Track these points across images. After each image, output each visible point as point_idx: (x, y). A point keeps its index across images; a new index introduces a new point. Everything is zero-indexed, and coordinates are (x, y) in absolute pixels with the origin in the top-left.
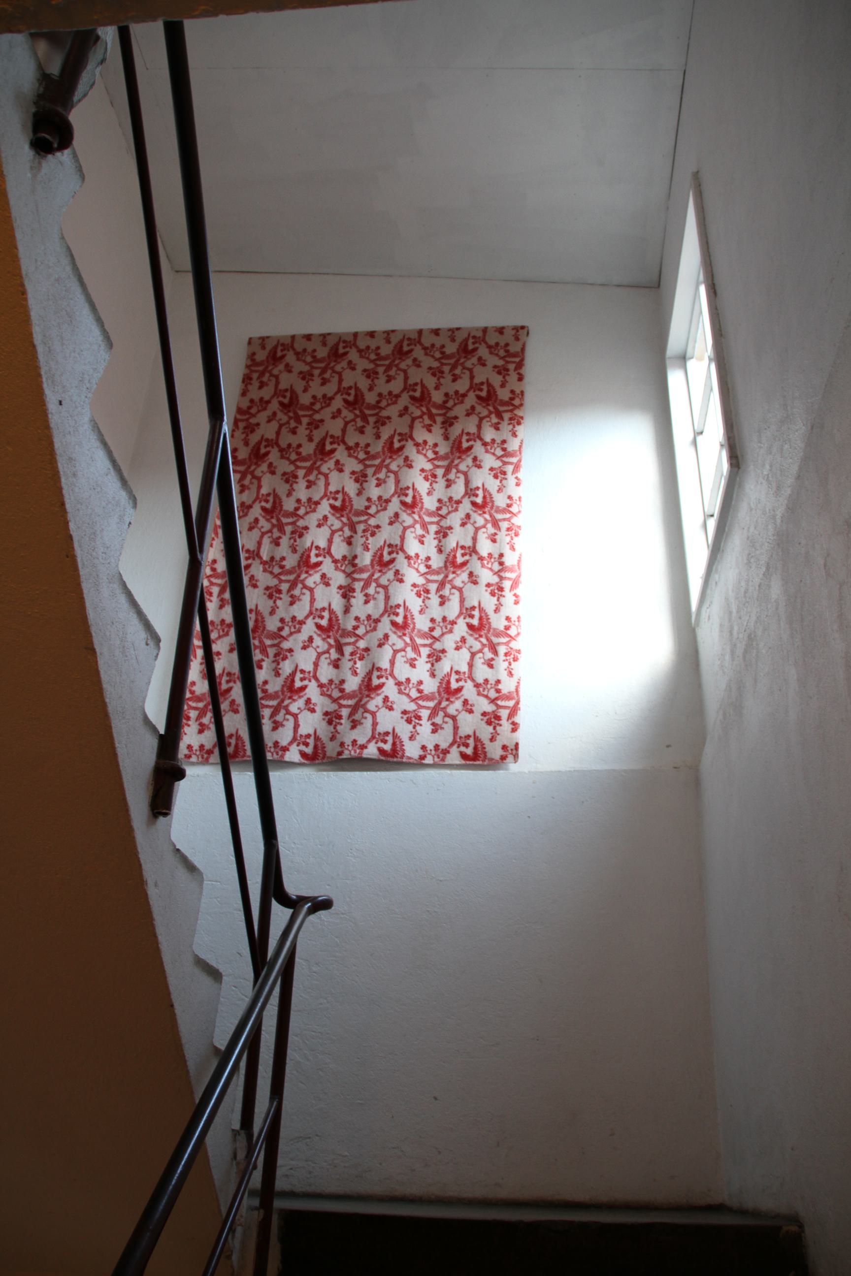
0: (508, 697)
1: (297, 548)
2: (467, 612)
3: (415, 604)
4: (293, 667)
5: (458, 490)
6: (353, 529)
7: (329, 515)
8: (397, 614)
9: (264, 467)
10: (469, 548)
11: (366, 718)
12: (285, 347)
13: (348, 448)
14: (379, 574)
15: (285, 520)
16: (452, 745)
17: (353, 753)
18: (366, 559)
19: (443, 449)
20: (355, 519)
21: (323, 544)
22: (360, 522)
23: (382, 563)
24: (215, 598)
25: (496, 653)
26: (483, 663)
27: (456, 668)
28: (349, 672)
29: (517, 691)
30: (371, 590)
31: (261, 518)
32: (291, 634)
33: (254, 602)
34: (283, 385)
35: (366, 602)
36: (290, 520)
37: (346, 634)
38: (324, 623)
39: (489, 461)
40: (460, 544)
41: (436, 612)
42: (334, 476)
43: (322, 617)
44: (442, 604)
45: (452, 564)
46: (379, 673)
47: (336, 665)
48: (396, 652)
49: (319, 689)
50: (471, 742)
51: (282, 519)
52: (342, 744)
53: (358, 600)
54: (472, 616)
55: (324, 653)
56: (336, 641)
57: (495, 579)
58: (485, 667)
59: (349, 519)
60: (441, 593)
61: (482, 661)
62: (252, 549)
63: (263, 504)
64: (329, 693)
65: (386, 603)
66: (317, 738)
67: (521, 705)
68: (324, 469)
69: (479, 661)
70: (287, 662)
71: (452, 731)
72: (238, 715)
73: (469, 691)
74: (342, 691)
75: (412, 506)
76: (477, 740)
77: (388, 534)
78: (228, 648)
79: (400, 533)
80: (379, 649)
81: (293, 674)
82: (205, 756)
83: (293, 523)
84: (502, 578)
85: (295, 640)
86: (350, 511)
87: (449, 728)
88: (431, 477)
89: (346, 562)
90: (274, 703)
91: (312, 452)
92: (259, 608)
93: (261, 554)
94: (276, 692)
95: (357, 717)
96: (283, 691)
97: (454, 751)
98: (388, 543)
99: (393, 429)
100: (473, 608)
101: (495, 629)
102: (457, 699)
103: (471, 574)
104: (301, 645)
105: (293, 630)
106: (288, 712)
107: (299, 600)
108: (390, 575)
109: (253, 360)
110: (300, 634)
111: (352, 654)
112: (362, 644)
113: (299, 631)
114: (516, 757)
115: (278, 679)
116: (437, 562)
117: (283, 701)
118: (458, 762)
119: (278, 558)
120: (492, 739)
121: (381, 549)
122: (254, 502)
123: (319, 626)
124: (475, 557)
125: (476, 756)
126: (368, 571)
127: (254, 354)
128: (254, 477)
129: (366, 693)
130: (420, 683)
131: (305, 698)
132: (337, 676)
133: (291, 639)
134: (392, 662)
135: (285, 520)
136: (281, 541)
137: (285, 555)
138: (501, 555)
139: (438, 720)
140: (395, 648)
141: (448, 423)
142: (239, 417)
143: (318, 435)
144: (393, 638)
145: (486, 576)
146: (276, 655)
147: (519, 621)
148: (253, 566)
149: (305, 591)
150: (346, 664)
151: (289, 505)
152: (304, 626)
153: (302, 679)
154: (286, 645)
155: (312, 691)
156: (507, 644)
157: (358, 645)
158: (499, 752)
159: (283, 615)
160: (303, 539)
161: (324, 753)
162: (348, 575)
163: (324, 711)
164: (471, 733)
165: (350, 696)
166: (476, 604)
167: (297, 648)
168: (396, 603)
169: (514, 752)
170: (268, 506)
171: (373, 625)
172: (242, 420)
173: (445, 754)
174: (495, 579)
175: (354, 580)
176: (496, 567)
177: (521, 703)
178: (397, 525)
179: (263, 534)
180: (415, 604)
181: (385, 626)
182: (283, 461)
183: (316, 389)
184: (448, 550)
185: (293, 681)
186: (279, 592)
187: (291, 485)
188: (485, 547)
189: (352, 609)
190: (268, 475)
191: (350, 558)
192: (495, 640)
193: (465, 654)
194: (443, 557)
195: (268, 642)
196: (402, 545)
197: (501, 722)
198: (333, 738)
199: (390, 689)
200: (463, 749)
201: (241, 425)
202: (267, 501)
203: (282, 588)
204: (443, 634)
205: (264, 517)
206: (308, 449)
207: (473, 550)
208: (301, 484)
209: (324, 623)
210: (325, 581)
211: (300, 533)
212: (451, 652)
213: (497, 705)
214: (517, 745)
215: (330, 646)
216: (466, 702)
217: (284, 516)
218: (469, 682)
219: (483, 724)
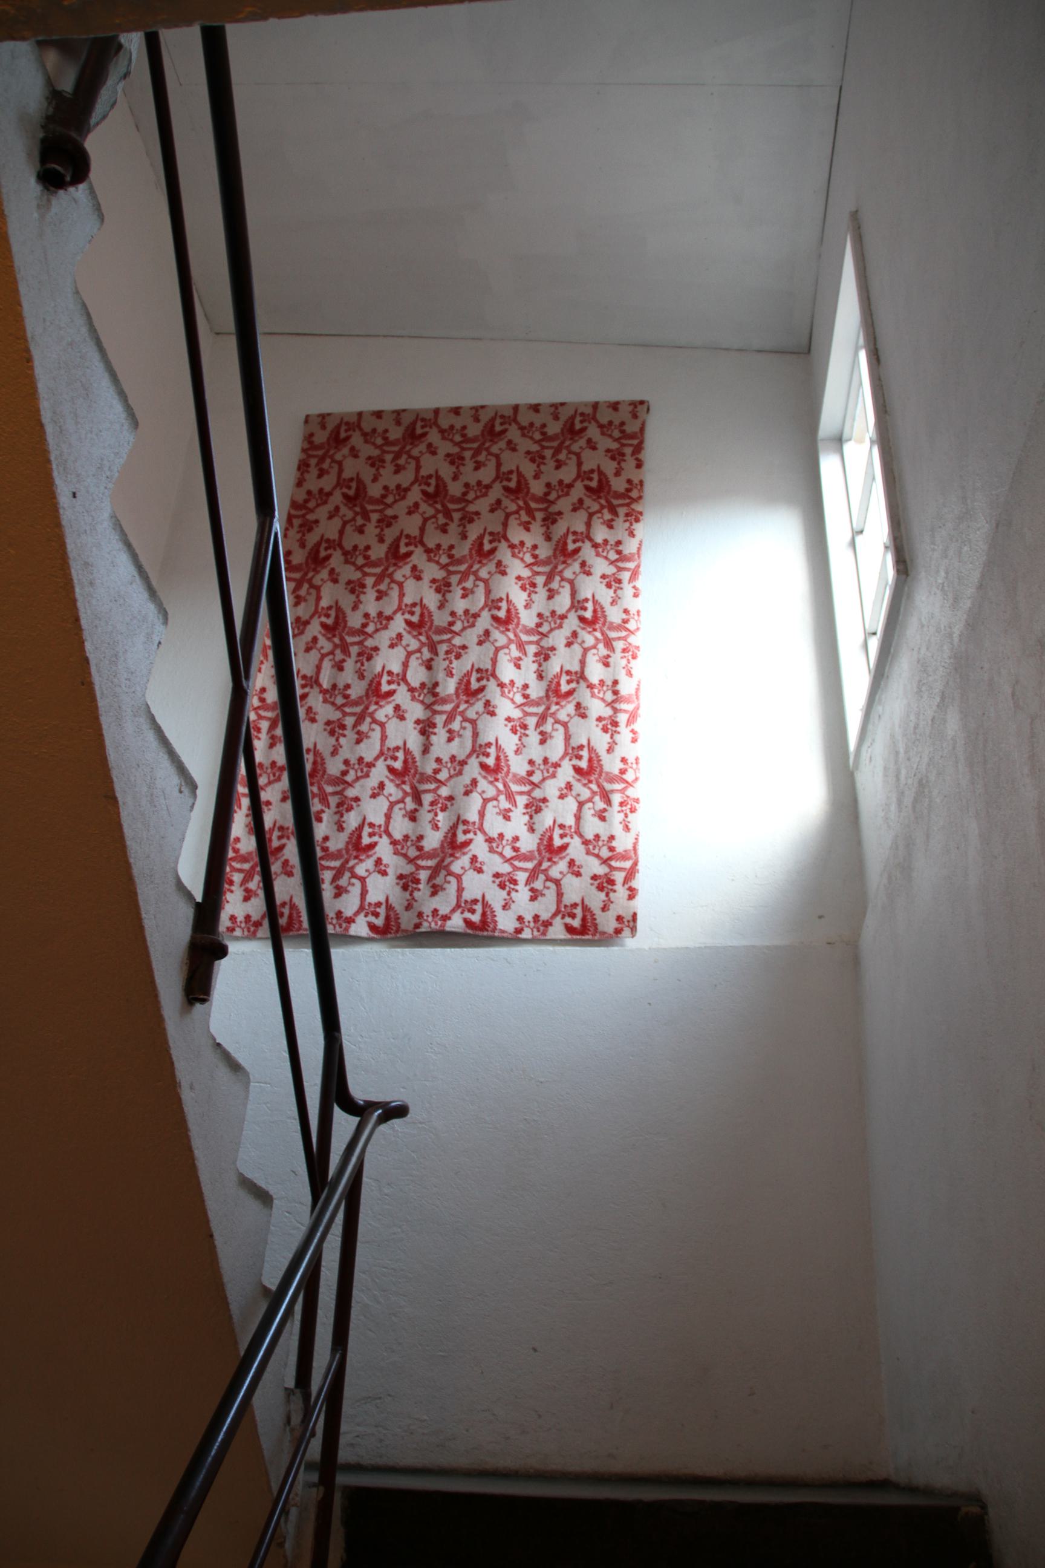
0: (624, 857)
1: (365, 674)
2: (573, 752)
3: (509, 742)
4: (360, 820)
5: (563, 602)
6: (433, 650)
7: (404, 633)
8: (488, 755)
9: (324, 574)
10: (576, 673)
11: (449, 882)
13: (428, 551)
14: (466, 706)
15: (350, 639)
16: (555, 915)
17: (433, 925)
18: (449, 687)
19: (544, 552)
20: (436, 638)
21: (396, 668)
22: (442, 642)
23: (469, 692)
24: (264, 735)
25: (609, 802)
26: (594, 815)
27: (559, 821)
28: (429, 826)
29: (635, 849)
30: (456, 725)
31: (320, 637)
32: (358, 779)
33: (312, 740)
34: (347, 474)
35: (450, 740)
36: (357, 639)
37: (424, 779)
38: (398, 765)
39: (601, 567)
40: (565, 669)
41: (536, 752)
42: (410, 585)
43: (395, 759)
44: (543, 742)
45: (554, 693)
46: (465, 827)
47: (413, 817)
48: (486, 801)
49: (391, 847)
50: (578, 911)
51: (347, 637)
52: (420, 915)
53: (439, 738)
54: (579, 758)
55: (398, 802)
56: (413, 787)
57: (607, 712)
58: (596, 819)
59: (428, 637)
60: (541, 728)
61: (592, 812)
62: (309, 675)
63: (323, 619)
64: (404, 851)
65: (474, 741)
66: (389, 907)
67: (640, 867)
68: (398, 576)
69: (588, 812)
70: (352, 814)
71: (555, 899)
72: (292, 879)
73: (576, 849)
74: (420, 849)
75: (506, 622)
76: (586, 909)
77: (476, 656)
78: (280, 796)
79: (491, 655)
80: (465, 798)
81: (360, 828)
82: (252, 929)
83: (360, 643)
84: (616, 711)
85: (362, 786)
86: (430, 628)
87: (551, 894)
88: (529, 586)
89: (425, 691)
90: (336, 864)
91: (383, 555)
92: (318, 747)
93: (321, 680)
94: (339, 851)
95: (438, 881)
96: (347, 850)
97: (558, 923)
98: (476, 667)
99: (483, 527)
100: (581, 747)
101: (607, 773)
102: (561, 858)
103: (578, 706)
104: (370, 792)
105: (359, 774)
106: (354, 875)
107: (368, 737)
108: (479, 706)
109: (311, 442)
110: (368, 780)
111: (432, 804)
112: (444, 792)
113: (367, 776)
114: (634, 930)
115: (341, 834)
116: (536, 690)
117: (347, 862)
118: (562, 937)
119: (341, 686)
120: (604, 909)
121: (468, 674)
122: (312, 617)
123: (391, 770)
124: (583, 684)
125: (585, 930)
126: (452, 701)
127: (312, 435)
128: (312, 586)
129: (450, 851)
130: (516, 839)
131: (374, 858)
132: (414, 831)
133: (357, 785)
134: (482, 814)
135: (350, 639)
136: (345, 664)
137: (350, 682)
138: (616, 682)
139: (538, 884)
140: (485, 796)
141: (550, 520)
142: (293, 512)
143: (390, 534)
144: (483, 784)
145: (597, 708)
146: (339, 805)
147: (637, 763)
148: (310, 696)
149: (374, 726)
150: (425, 816)
151: (355, 620)
152: (373, 770)
153: (371, 835)
154: (351, 793)
155: (384, 849)
156: (622, 791)
157: (439, 792)
158: (613, 924)
159: (348, 756)
160: (372, 662)
161: (398, 925)
162: (428, 707)
163: (398, 873)
164: (578, 901)
165: (430, 856)
166: (585, 743)
167: (365, 796)
168: (486, 741)
169: (631, 924)
170: (330, 621)
171: (458, 768)
172: (297, 517)
173: (546, 926)
174: (607, 712)
175: (435, 712)
176: (609, 697)
177: (640, 864)
178: (487, 645)
179: (323, 656)
180: (509, 742)
181: (473, 769)
182: (347, 566)
183: (388, 478)
184: (550, 676)
185: (360, 837)
186: (343, 727)
187: (358, 597)
188: (595, 672)
189: (432, 748)
190: (329, 584)
191: (429, 685)
192: (608, 787)
193: (571, 804)
194: (544, 684)
195: (329, 789)
196: (494, 670)
197: (615, 888)
198: (408, 907)
199: (479, 847)
200: (568, 920)
201: (296, 522)
202: (328, 616)
203: (346, 723)
204: (544, 779)
205: (324, 635)
206: (378, 551)
207: (580, 676)
208: (370, 595)
209: (398, 765)
210: (399, 713)
211: (368, 655)
212: (554, 802)
213: (610, 866)
214: (635, 915)
215: (406, 794)
216: (572, 863)
217: (348, 634)
218: (576, 838)
219: (593, 889)
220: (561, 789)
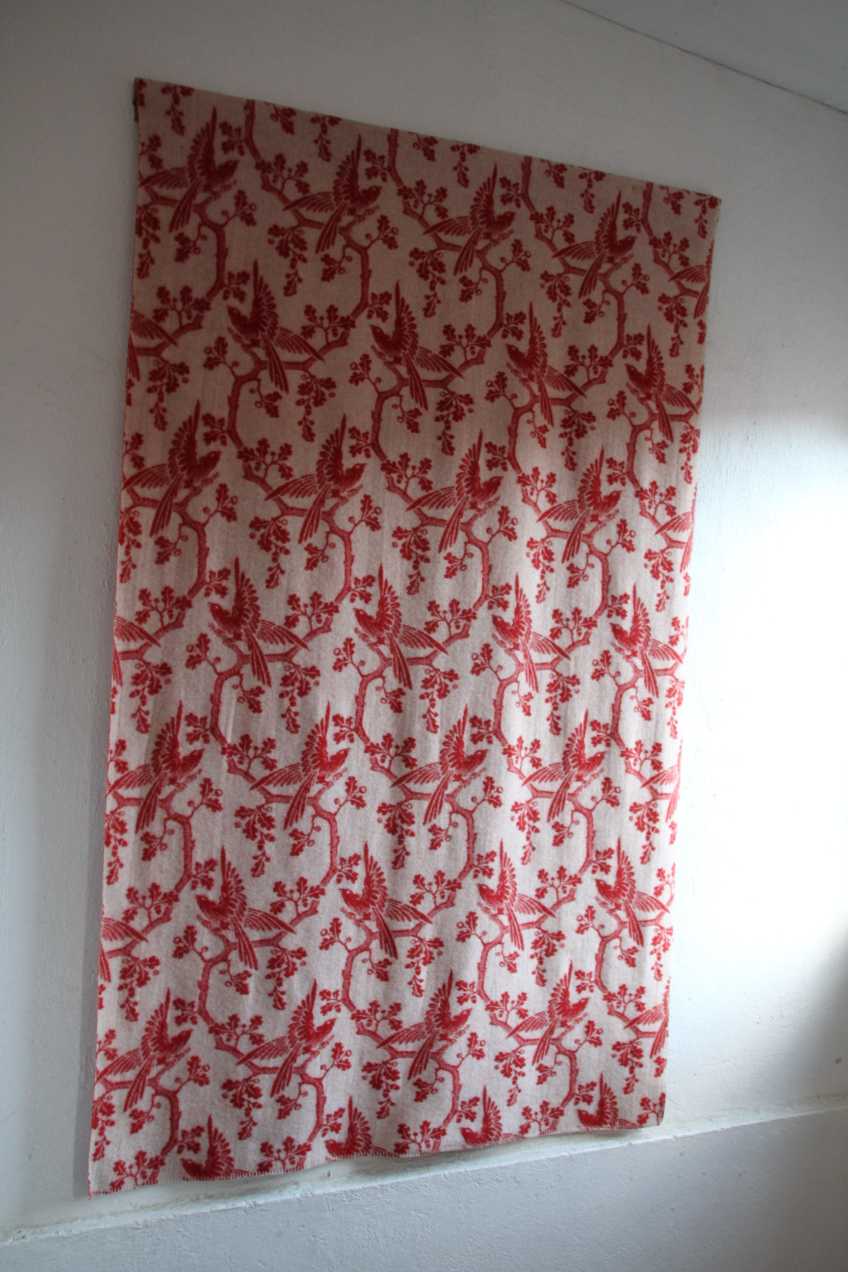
0: (653, 1017)
4: (307, 989)
5: (590, 595)
6: (405, 678)
7: (356, 639)
11: (442, 1080)
12: (242, 138)
13: (388, 467)
14: (456, 784)
15: (268, 648)
16: (566, 1100)
17: (424, 1148)
18: (430, 750)
19: (565, 491)
20: (408, 651)
21: (346, 710)
22: (416, 660)
23: (464, 762)
28: (409, 990)
29: (665, 1003)
30: (442, 820)
32: (300, 917)
33: (218, 844)
34: (235, 263)
35: (434, 845)
36: (279, 648)
37: (398, 911)
39: (647, 537)
40: (591, 718)
41: (548, 858)
42: (361, 535)
43: (353, 877)
44: (558, 841)
46: (461, 993)
47: (382, 973)
48: (487, 947)
50: (595, 1093)
52: (403, 1130)
53: (418, 842)
54: (606, 869)
56: (382, 924)
60: (557, 819)
64: (372, 1028)
65: (470, 849)
66: (354, 1114)
67: (670, 1028)
68: (342, 520)
69: (613, 952)
70: (296, 977)
71: (568, 1078)
72: (207, 1087)
73: (596, 1008)
74: (396, 1025)
76: (605, 1090)
77: (468, 696)
79: (494, 696)
80: (460, 944)
82: (149, 1172)
84: (656, 795)
85: (308, 930)
86: (396, 629)
87: (563, 1071)
88: (543, 558)
89: (392, 751)
90: (277, 1062)
91: (312, 469)
92: (228, 858)
93: (222, 729)
94: (280, 1040)
95: (426, 1075)
96: (291, 1037)
97: (570, 1110)
98: (471, 714)
100: (608, 853)
101: (641, 895)
102: (577, 1021)
103: (607, 784)
104: (320, 940)
106: (306, 1079)
107: (311, 843)
108: (476, 787)
109: (156, 162)
110: (315, 917)
111: (412, 953)
112: (428, 932)
113: (314, 911)
114: (660, 1115)
115: (281, 1013)
116: (550, 755)
117: (293, 1058)
118: (577, 1130)
119: (258, 740)
120: (627, 1090)
121: (459, 728)
124: (615, 750)
125: (602, 1116)
126: (435, 777)
127: (155, 142)
128: (187, 522)
129: (441, 1031)
130: (523, 997)
132: (386, 996)
133: (299, 928)
134: (482, 968)
135: (268, 648)
136: (262, 698)
137: (273, 735)
139: (547, 1060)
140: (486, 940)
141: (577, 426)
142: (138, 341)
143: (324, 421)
144: (484, 922)
145: (632, 790)
146: (273, 963)
148: (205, 755)
150: (402, 974)
151: (273, 610)
152: (322, 899)
153: (325, 1010)
154: (290, 942)
155: (344, 1030)
156: (656, 921)
157: (421, 934)
158: (638, 1110)
159: (280, 876)
160: (309, 698)
161: (368, 1138)
162: (399, 782)
163: (364, 1063)
164: (596, 1079)
165: (412, 1035)
166: (614, 847)
167: (313, 947)
168: (488, 850)
169: (658, 1108)
170: (227, 603)
171: (447, 893)
172: (146, 351)
173: (556, 1117)
175: (412, 795)
176: (648, 771)
177: (670, 1023)
178: (487, 673)
179: (222, 677)
181: (468, 898)
183: (316, 293)
184: (571, 730)
185: (310, 1016)
186: (268, 822)
188: (633, 729)
191: (398, 741)
192: (640, 915)
193: (592, 939)
195: (255, 935)
197: (642, 1060)
198: (382, 1114)
199: (479, 1020)
200: (583, 1106)
201: (146, 364)
203: (273, 814)
204: (559, 903)
205: (219, 633)
206: (305, 460)
207: (611, 733)
211: (301, 682)
212: (572, 939)
213: (637, 1031)
214: (663, 1096)
216: (590, 1026)
218: (597, 991)
220: (208, 351)
